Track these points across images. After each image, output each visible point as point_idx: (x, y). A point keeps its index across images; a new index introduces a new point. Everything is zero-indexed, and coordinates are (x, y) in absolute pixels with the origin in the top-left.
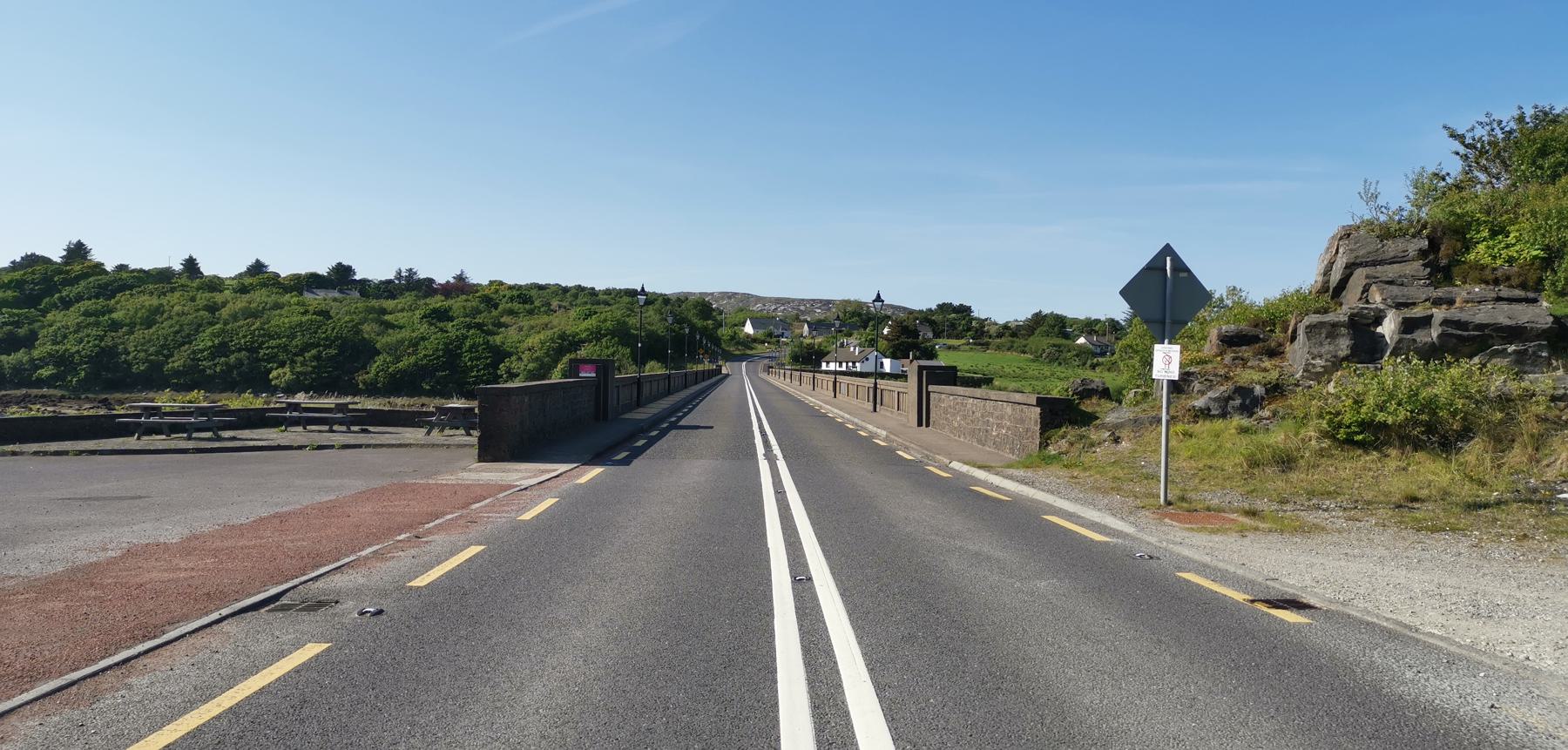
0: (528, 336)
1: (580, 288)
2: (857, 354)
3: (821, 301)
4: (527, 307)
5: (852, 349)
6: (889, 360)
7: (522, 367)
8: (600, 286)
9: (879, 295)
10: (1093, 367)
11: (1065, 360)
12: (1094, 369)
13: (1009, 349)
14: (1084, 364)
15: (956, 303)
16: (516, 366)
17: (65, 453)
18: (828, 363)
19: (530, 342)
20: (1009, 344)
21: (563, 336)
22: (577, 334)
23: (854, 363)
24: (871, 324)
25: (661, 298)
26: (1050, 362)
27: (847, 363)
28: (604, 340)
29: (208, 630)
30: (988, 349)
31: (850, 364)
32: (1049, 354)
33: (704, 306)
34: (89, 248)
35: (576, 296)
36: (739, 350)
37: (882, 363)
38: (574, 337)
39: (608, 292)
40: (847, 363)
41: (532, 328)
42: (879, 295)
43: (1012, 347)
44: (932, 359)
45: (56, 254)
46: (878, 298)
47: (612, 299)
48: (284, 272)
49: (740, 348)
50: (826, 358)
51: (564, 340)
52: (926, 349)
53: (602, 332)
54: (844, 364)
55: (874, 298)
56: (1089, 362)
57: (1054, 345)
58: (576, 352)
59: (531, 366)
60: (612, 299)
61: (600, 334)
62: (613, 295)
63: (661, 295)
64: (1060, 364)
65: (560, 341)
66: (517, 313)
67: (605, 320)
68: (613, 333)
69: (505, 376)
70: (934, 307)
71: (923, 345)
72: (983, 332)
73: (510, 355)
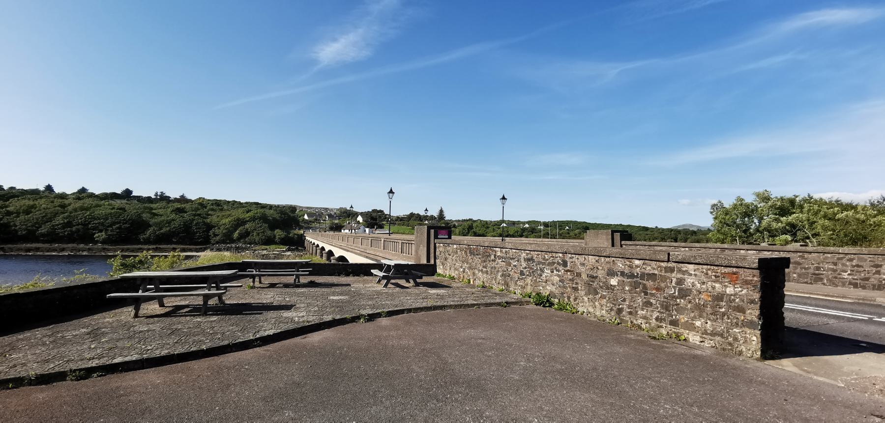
0: (222, 219)
1: (235, 202)
3: (324, 208)
4: (220, 207)
16: (217, 231)
19: (224, 221)
20: (403, 224)
21: (238, 219)
23: (355, 230)
33: (293, 209)
34: (445, 215)
35: (233, 204)
37: (365, 230)
38: (243, 219)
39: (247, 203)
41: (223, 216)
42: (352, 206)
50: (344, 228)
52: (380, 224)
59: (224, 231)
67: (257, 213)
68: (260, 218)
70: (371, 210)
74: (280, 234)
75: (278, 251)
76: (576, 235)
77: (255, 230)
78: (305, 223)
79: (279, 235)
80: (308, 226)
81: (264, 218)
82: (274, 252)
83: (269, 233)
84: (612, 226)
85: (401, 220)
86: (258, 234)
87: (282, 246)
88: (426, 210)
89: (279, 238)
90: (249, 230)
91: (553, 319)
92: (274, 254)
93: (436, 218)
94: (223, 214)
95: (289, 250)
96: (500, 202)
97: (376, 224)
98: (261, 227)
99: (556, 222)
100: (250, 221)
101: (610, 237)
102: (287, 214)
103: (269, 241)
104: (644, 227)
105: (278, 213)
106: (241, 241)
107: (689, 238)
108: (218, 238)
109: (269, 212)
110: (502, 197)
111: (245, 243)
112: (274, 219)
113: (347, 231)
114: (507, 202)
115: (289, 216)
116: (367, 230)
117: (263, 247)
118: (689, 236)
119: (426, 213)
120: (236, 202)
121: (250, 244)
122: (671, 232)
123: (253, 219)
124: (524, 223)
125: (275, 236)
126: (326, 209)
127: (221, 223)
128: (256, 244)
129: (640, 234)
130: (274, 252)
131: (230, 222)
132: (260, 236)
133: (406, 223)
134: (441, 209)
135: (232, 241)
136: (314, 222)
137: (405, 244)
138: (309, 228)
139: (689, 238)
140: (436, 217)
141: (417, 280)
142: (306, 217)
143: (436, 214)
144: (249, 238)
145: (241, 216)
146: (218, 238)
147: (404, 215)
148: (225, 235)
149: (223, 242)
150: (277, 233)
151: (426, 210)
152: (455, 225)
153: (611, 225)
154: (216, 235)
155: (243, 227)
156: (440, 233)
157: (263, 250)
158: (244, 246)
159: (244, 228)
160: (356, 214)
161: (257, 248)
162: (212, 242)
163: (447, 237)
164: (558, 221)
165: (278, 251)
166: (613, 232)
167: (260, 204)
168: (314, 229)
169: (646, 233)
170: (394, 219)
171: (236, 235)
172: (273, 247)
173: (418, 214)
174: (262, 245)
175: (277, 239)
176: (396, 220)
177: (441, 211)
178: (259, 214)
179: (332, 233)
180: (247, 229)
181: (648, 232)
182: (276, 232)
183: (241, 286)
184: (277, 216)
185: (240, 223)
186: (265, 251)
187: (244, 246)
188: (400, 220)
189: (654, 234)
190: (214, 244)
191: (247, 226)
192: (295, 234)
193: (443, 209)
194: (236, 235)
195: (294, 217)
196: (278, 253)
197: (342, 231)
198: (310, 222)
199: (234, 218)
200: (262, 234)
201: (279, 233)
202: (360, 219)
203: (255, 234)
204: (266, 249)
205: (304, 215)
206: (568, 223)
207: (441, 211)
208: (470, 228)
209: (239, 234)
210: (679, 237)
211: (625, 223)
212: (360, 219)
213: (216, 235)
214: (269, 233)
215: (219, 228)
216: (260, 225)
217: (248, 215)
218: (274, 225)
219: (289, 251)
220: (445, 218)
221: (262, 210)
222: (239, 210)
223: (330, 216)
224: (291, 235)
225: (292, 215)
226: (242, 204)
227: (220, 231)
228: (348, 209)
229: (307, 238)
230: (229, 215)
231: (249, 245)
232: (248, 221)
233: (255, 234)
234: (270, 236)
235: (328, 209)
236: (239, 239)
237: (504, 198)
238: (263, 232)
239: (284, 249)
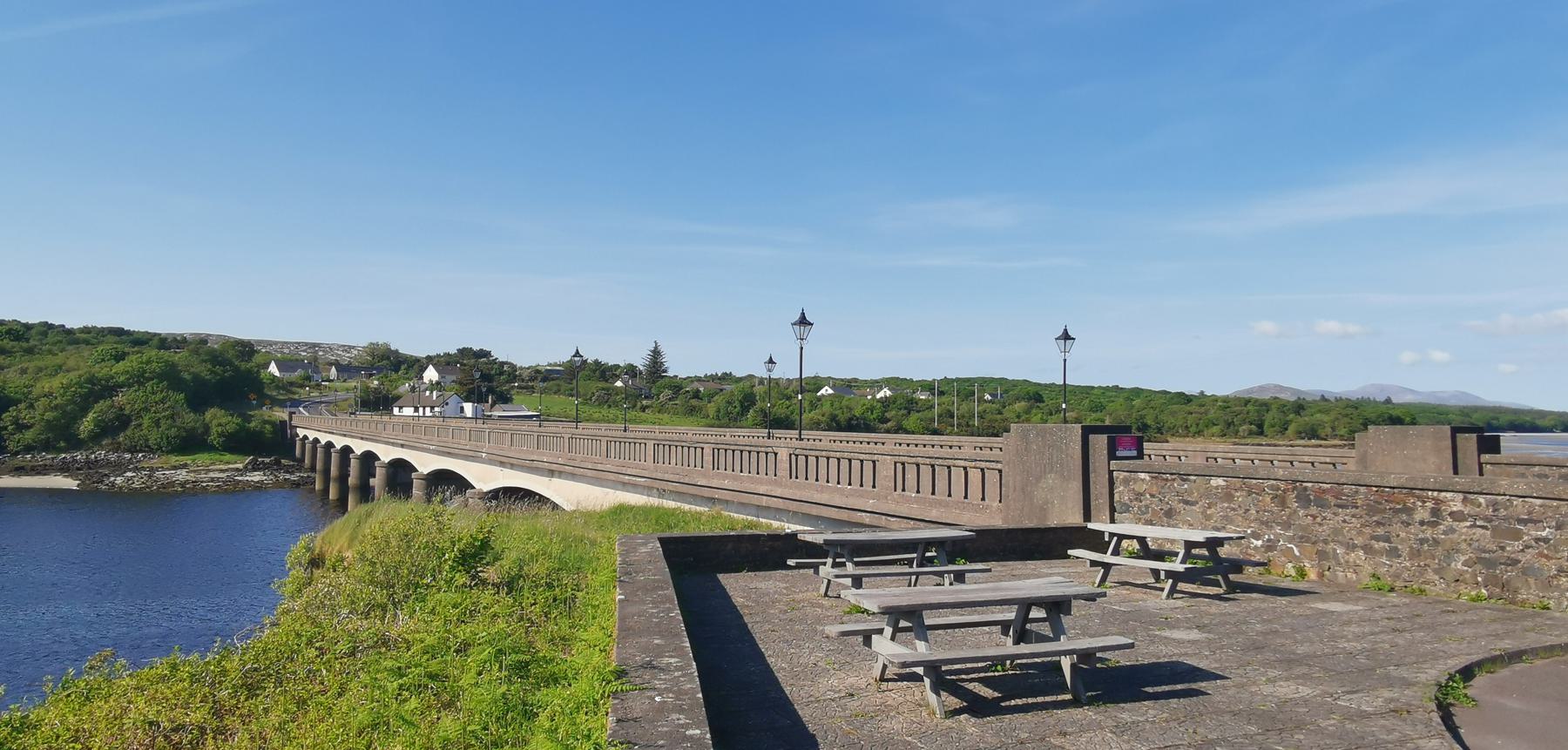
0: (37, 380)
1: (48, 327)
2: (435, 398)
3: (306, 344)
4: (25, 345)
5: (428, 393)
6: (470, 404)
7: (38, 417)
8: (73, 323)
9: (577, 352)
10: (643, 409)
11: (614, 402)
12: (644, 411)
13: (555, 393)
14: (634, 406)
15: (476, 348)
16: (26, 416)
17: (1321, 446)
18: (401, 408)
19: (46, 385)
20: (555, 389)
21: (92, 380)
22: (113, 378)
23: (432, 408)
24: (403, 367)
25: (157, 338)
26: (599, 405)
27: (424, 408)
28: (149, 385)
29: (1459, 455)
30: (534, 392)
31: (428, 409)
32: (599, 396)
33: (246, 349)
34: (666, 365)
35: (45, 334)
36: (282, 394)
37: (462, 408)
38: (107, 381)
39: (86, 330)
40: (424, 408)
41: (40, 370)
42: (577, 352)
43: (559, 390)
44: (506, 403)
45: (728, 373)
46: (577, 354)
47: (93, 338)
48: (739, 375)
49: (281, 392)
50: (399, 403)
51: (94, 384)
52: (502, 392)
53: (147, 375)
54: (421, 409)
55: (574, 353)
56: (639, 405)
57: (603, 389)
58: (111, 398)
59: (49, 415)
60: (93, 338)
61: (143, 377)
62: (91, 336)
63: (155, 334)
64: (610, 406)
65: (90, 386)
66: (10, 352)
67: (149, 362)
68: (161, 377)
69: (10, 427)
70: (453, 351)
71: (498, 389)
72: (515, 376)
73: (16, 402)
74: (224, 420)
75: (222, 471)
76: (1018, 417)
77: (146, 410)
78: (278, 388)
79: (220, 425)
80: (287, 395)
81: (170, 377)
82: (212, 475)
83: (189, 418)
84: (1095, 391)
85: (544, 380)
86: (157, 423)
87: (228, 457)
88: (771, 361)
89: (220, 435)
90: (127, 412)
91: (1160, 647)
92: (212, 480)
93: (641, 373)
94: (41, 364)
95: (255, 467)
96: (790, 333)
97: (491, 391)
98: (163, 401)
99: (953, 380)
100: (130, 386)
101: (1449, 443)
102: (231, 364)
103: (191, 443)
104: (1181, 394)
105: (205, 361)
106: (104, 443)
107: (1291, 421)
108: (29, 435)
109: (179, 357)
110: (797, 317)
111: (117, 448)
112: (196, 377)
113: (409, 411)
114: (1076, 349)
115: (237, 369)
116: (469, 408)
117: (174, 459)
118: (1292, 416)
119: (770, 370)
120: (51, 326)
121: (133, 450)
122: (1246, 405)
123: (139, 379)
124: (877, 384)
125: (207, 429)
126: (314, 345)
127: (36, 391)
128: (151, 451)
129: (1173, 414)
130: (212, 475)
131: (66, 388)
132: (163, 427)
133: (564, 386)
134: (656, 348)
135: (76, 443)
136: (302, 386)
137: (613, 443)
138: (296, 403)
139: (1291, 421)
140: (642, 368)
141: (1230, 576)
142: (273, 369)
143: (640, 361)
144: (129, 432)
145: (102, 371)
146: (29, 435)
147: (550, 365)
148: (50, 426)
149: (47, 446)
150: (214, 417)
151: (771, 361)
152: (698, 391)
153: (1093, 388)
154: (21, 427)
155: (108, 402)
156: (1120, 444)
157: (175, 468)
158: (113, 457)
159: (112, 406)
160: (415, 366)
161: (156, 461)
162: (11, 446)
163: (1134, 453)
164: (958, 380)
165: (222, 471)
166: (1455, 431)
167: (128, 333)
168: (311, 405)
169: (1188, 408)
170: (525, 374)
171: (86, 425)
172: (203, 458)
173: (597, 363)
174: (169, 452)
175: (213, 438)
176: (532, 379)
177: (656, 353)
178: (155, 364)
179: (365, 416)
180: (121, 409)
181: (1192, 407)
182: (208, 415)
183: (1131, 646)
184: (203, 370)
185: (99, 390)
186: (184, 472)
187: (113, 457)
188: (544, 378)
189: (1206, 413)
190: (17, 453)
191: (120, 399)
192: (266, 422)
193: (663, 348)
194: (86, 425)
195: (249, 371)
196: (221, 475)
197: (396, 410)
198: (292, 384)
199: (80, 376)
200: (169, 422)
201: (218, 420)
202: (431, 374)
203: (146, 422)
204: (185, 466)
205: (267, 366)
206: (985, 382)
207: (656, 353)
208: (748, 400)
209: (97, 423)
210: (1269, 418)
211: (1561, 410)
212: (431, 374)
213: (21, 427)
214: (189, 418)
215: (31, 406)
216: (158, 397)
217: (121, 366)
218: (200, 396)
219: (254, 470)
220: (665, 371)
221: (164, 354)
222: (86, 354)
223: (341, 368)
224: (253, 425)
225: (244, 366)
226: (70, 332)
227: (38, 415)
228: (762, 372)
229: (301, 432)
230: (59, 369)
231: (128, 456)
232: (121, 386)
233: (146, 422)
234: (194, 429)
235: (318, 345)
236: (95, 438)
237: (803, 321)
238: (172, 417)
239: (240, 466)
